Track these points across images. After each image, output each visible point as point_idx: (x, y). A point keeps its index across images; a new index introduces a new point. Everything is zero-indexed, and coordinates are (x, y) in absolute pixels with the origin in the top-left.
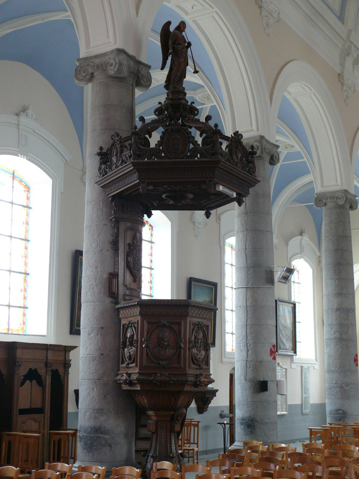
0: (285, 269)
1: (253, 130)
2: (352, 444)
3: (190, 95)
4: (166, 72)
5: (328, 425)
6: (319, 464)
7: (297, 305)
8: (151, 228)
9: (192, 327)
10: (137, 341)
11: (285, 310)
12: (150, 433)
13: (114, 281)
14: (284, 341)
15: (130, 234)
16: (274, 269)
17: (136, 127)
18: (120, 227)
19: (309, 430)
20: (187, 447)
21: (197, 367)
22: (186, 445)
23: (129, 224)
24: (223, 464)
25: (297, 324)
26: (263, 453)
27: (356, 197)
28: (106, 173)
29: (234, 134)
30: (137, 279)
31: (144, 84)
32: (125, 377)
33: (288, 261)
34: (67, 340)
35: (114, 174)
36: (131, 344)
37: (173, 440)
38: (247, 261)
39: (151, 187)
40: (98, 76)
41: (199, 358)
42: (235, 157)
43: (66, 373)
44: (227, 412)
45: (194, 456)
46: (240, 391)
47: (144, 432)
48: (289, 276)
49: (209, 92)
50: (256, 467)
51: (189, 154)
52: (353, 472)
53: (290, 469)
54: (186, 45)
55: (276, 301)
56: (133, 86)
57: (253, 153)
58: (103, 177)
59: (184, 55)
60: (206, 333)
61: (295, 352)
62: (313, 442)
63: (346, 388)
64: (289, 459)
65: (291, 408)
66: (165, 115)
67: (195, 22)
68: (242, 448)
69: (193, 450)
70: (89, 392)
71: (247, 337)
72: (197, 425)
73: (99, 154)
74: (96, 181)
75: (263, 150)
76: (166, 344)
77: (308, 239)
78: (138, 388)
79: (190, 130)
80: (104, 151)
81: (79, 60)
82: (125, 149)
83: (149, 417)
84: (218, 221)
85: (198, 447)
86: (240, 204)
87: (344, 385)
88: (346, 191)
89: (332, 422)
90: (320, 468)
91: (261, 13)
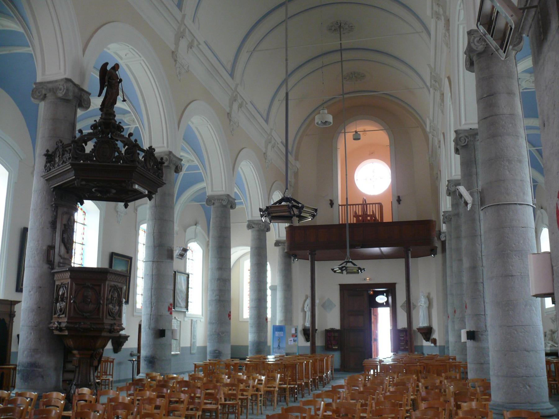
0: (182, 249)
1: (164, 147)
2: (223, 374)
3: (118, 118)
4: (101, 99)
5: (208, 361)
6: (199, 388)
7: (190, 276)
8: (84, 214)
9: (109, 288)
10: (67, 298)
11: (181, 279)
12: (74, 367)
13: (52, 252)
14: (180, 301)
15: (65, 217)
16: (173, 248)
17: (75, 137)
18: (58, 211)
19: (194, 365)
20: (104, 377)
21: (112, 318)
22: (103, 376)
23: (65, 210)
24: (128, 389)
25: (190, 289)
26: (160, 381)
27: (235, 200)
28: (50, 170)
29: (149, 148)
30: (70, 251)
31: (84, 106)
32: (56, 325)
33: (58, 152)
34: (13, 297)
35: (55, 171)
36: (62, 300)
37: (92, 372)
38: (154, 242)
39: (84, 183)
40: (50, 96)
41: (114, 312)
42: (148, 165)
43: (11, 321)
44: (136, 352)
45: (108, 384)
46: (145, 337)
47: (70, 366)
48: (184, 254)
49: (134, 117)
50: (153, 391)
51: (114, 160)
52: (222, 392)
53: (178, 392)
54: (118, 80)
55: (175, 272)
56: (76, 107)
57: (162, 163)
58: (48, 173)
59: (116, 88)
60: (120, 293)
61: (187, 310)
62: (197, 373)
63: (221, 335)
64: (178, 386)
65: (183, 349)
66: (99, 130)
67: (127, 65)
68: (145, 378)
69: (109, 380)
70: (28, 336)
71: (151, 297)
72: (113, 362)
73: (45, 155)
74: (42, 175)
75: (171, 161)
76: (89, 300)
77: (200, 228)
78: (66, 333)
79: (116, 142)
80: (50, 153)
81: (35, 83)
82: (66, 153)
83: (74, 355)
84: (136, 212)
85: (112, 378)
86: (150, 200)
87: (220, 333)
88: (228, 196)
89: (211, 359)
90: (199, 390)
91: (175, 65)
